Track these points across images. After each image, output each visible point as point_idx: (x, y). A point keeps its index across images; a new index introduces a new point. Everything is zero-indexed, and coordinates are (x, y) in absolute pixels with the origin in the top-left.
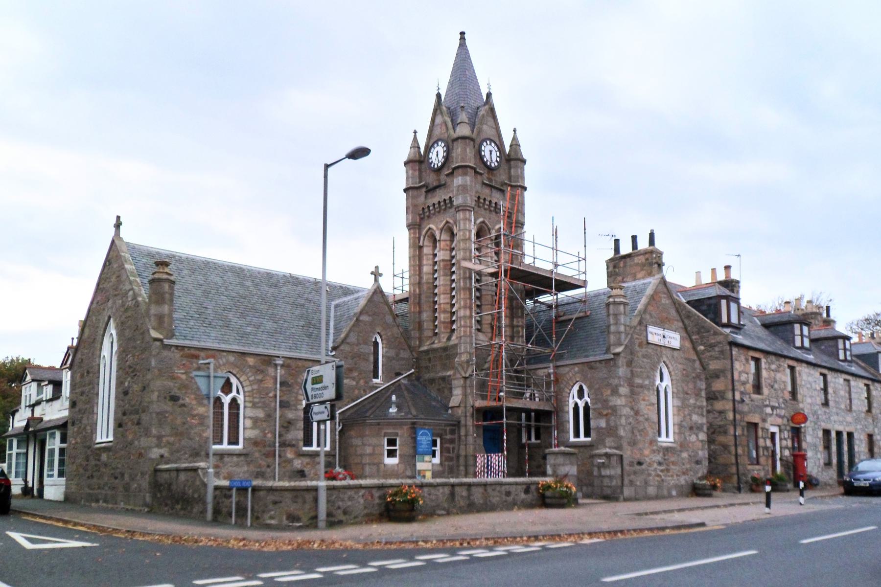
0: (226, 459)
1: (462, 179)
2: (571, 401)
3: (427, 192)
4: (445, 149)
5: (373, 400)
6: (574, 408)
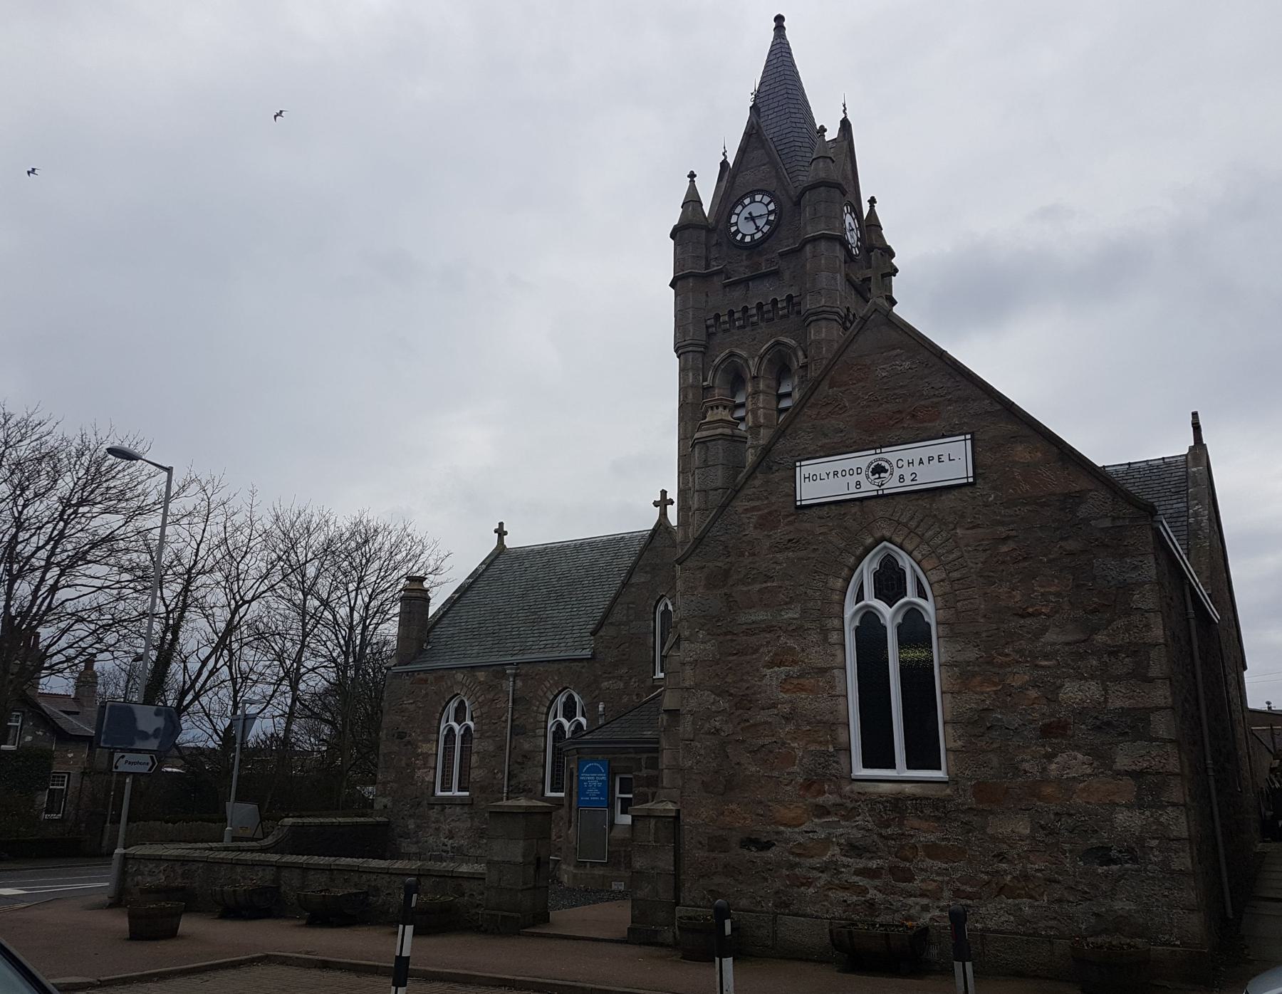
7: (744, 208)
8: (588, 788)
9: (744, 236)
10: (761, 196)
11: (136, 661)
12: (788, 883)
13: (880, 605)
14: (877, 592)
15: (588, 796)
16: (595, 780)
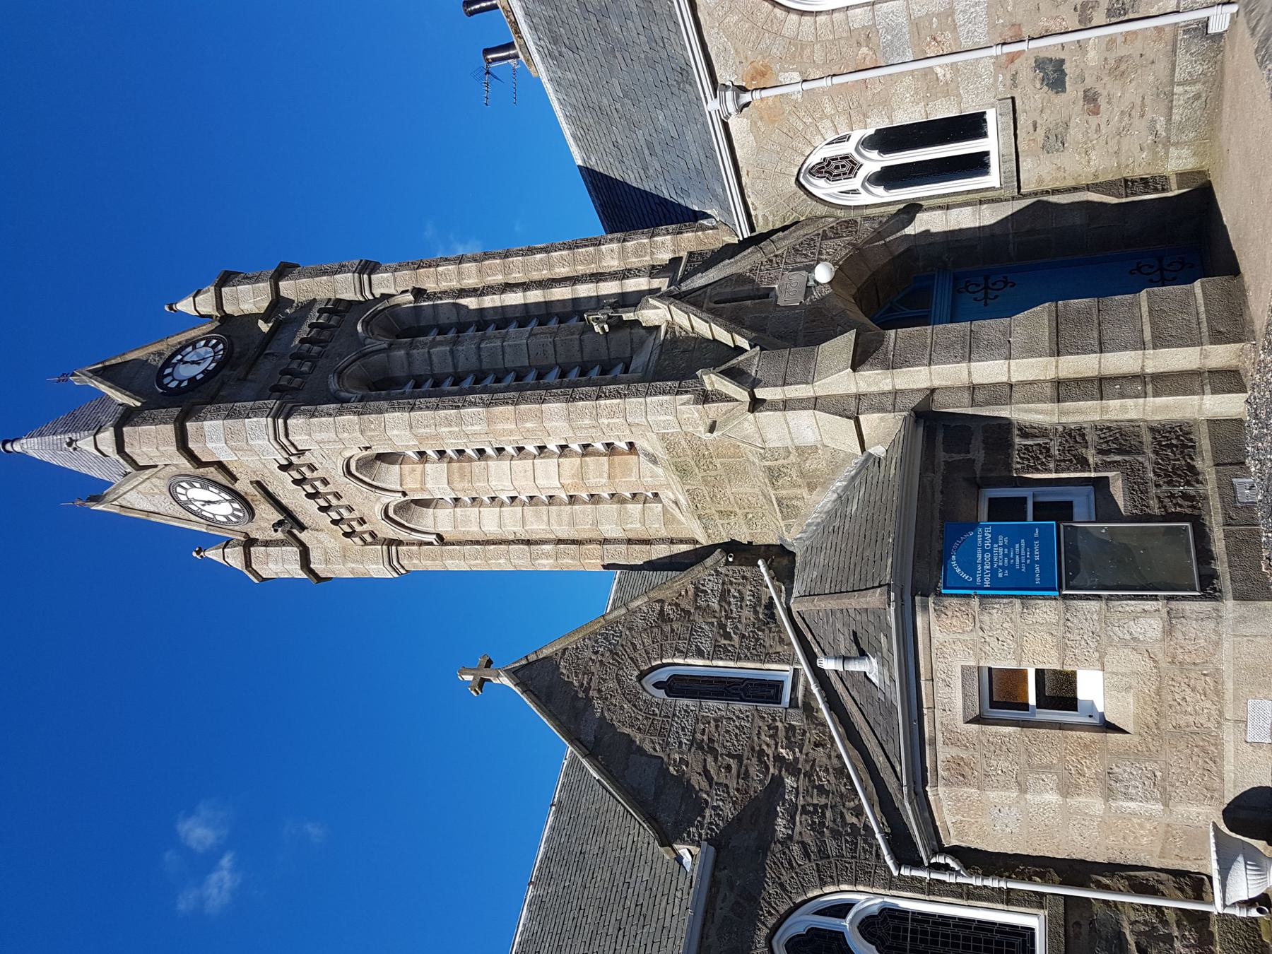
0: (771, 548)
2: (864, 199)
3: (302, 528)
5: (709, 694)
6: (889, 187)
8: (1011, 567)
11: (745, 88)
12: (1118, 386)
13: (862, 174)
15: (1030, 568)
16: (991, 551)
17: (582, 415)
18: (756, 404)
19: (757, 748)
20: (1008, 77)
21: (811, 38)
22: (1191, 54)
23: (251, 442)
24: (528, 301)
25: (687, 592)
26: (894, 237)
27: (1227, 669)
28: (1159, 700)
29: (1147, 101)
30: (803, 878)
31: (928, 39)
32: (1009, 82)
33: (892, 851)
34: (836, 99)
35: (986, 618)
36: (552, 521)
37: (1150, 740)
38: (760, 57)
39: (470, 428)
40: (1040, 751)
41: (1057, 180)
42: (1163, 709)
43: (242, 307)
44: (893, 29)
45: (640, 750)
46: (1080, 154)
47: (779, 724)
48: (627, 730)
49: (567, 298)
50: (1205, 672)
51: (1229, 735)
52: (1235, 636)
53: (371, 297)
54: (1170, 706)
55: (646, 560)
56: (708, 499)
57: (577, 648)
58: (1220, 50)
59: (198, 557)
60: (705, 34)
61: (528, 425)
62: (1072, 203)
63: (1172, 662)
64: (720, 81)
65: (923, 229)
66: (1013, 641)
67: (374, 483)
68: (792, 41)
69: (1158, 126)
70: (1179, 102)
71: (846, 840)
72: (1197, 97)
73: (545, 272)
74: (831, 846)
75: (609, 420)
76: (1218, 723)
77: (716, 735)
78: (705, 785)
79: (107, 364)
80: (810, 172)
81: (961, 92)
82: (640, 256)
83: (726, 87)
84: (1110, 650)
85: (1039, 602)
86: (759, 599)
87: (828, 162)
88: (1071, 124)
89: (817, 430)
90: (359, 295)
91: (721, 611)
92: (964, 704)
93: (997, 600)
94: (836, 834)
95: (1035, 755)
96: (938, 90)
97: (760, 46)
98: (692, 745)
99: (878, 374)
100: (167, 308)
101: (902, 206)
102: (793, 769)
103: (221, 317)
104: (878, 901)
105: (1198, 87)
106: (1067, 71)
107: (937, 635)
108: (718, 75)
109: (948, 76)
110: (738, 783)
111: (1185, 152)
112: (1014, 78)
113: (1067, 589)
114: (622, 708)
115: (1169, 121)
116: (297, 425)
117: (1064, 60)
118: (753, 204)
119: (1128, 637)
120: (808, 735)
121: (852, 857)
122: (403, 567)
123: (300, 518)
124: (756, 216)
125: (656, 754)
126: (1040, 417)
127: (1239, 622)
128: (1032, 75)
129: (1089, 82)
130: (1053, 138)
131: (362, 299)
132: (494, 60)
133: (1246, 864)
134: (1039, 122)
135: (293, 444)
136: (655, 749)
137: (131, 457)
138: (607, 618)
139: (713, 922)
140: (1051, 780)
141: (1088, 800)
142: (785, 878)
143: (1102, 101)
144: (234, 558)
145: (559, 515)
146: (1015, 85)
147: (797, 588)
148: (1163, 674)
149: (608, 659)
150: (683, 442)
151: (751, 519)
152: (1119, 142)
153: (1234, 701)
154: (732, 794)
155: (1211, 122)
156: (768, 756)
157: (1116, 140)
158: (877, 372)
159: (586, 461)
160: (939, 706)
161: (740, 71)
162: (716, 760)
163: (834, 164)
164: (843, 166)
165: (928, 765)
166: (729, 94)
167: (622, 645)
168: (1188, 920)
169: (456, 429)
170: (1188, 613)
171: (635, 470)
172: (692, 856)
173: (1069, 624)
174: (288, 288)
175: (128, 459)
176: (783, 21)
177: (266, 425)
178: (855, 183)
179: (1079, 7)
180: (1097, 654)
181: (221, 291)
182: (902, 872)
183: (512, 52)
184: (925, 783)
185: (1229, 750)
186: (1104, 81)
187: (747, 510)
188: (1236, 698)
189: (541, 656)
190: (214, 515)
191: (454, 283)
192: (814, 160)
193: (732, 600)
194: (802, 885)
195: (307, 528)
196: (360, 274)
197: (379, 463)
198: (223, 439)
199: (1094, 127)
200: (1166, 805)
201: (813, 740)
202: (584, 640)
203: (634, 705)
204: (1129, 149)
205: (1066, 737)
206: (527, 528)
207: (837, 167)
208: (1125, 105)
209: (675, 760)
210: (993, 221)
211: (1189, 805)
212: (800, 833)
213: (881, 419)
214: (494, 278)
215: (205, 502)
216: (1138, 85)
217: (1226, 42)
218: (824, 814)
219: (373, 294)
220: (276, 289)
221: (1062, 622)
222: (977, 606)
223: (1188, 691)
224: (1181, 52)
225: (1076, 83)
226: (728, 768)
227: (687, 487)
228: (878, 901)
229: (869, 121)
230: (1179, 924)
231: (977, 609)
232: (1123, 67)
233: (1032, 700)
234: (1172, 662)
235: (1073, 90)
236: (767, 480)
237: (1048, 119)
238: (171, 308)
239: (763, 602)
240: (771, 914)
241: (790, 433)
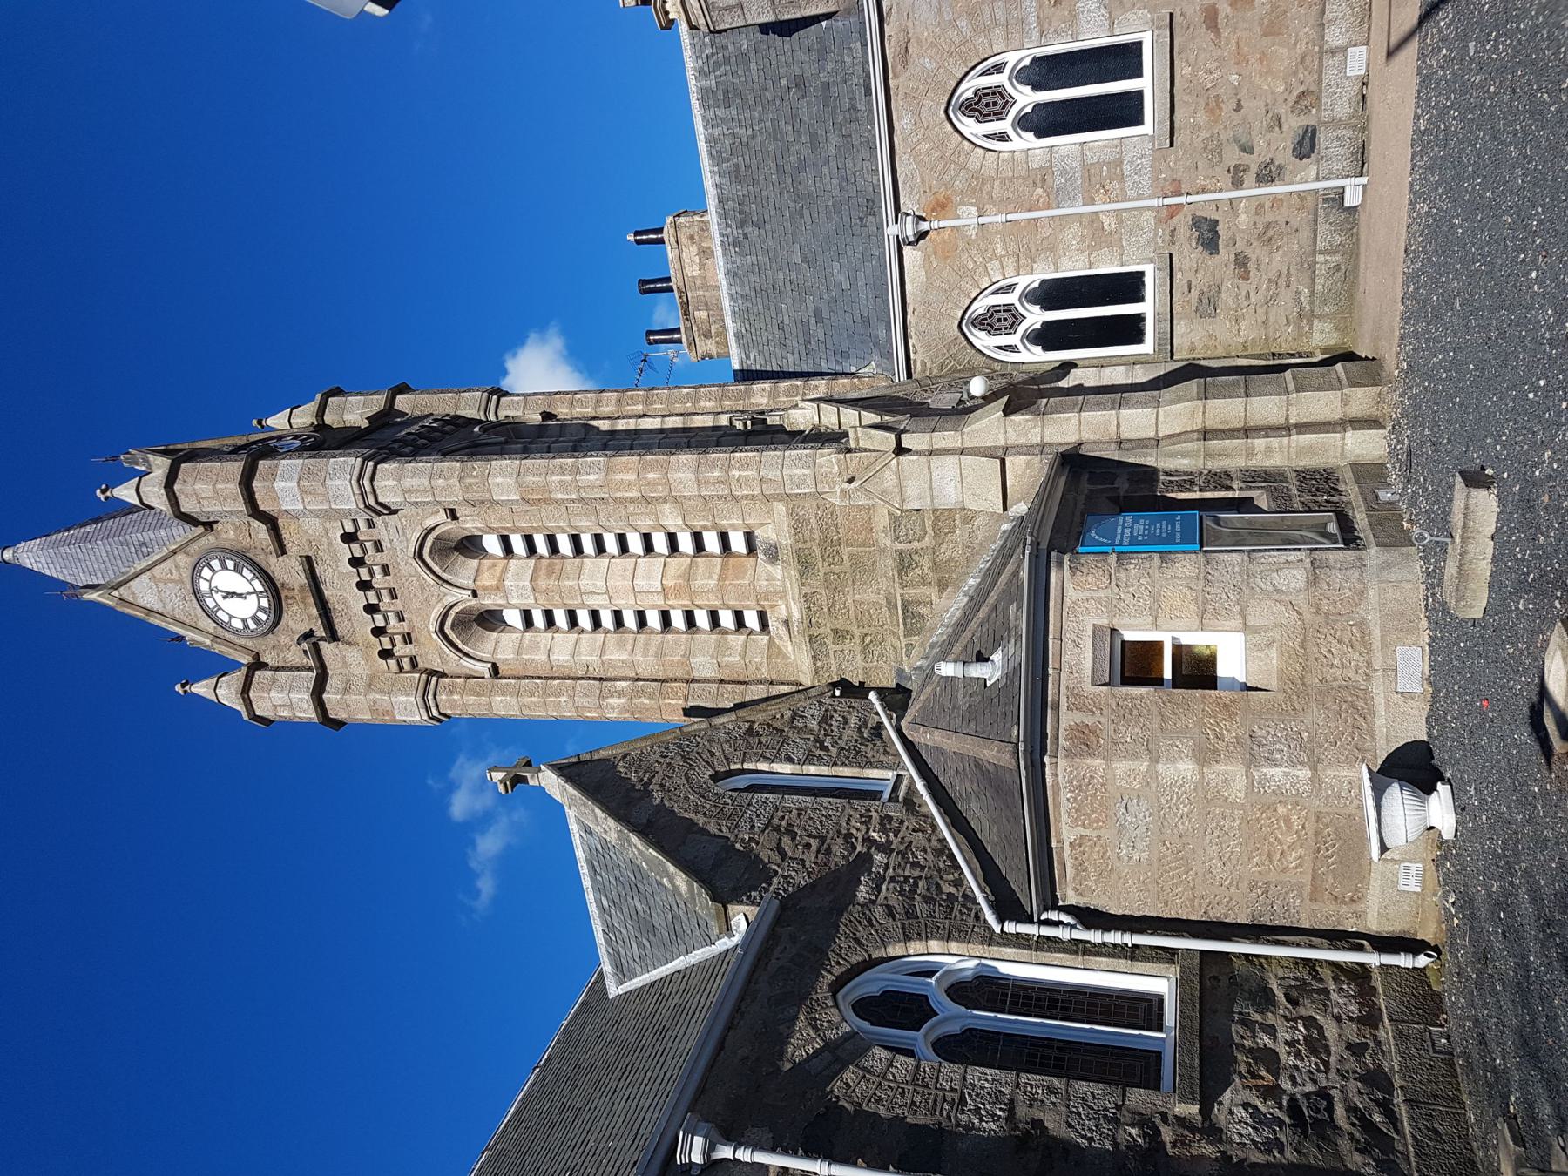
1: (283, 479)
3: (333, 636)
4: (230, 564)
7: (220, 608)
9: (260, 608)
10: (201, 580)
13: (1021, 329)
14: (1157, 1042)
17: (713, 467)
18: (900, 450)
19: (844, 831)
20: (1167, 232)
21: (992, 173)
22: (1330, 224)
23: (328, 482)
24: (665, 426)
25: (782, 716)
26: (1048, 386)
27: (1374, 618)
28: (1302, 651)
29: (1293, 271)
30: (884, 935)
31: (1098, 186)
32: (1167, 238)
33: (994, 907)
34: (1008, 240)
35: (1123, 575)
36: (637, 651)
37: (1295, 698)
38: (943, 187)
39: (585, 477)
40: (1175, 714)
41: (1208, 348)
42: (1308, 663)
43: (345, 417)
44: (1067, 173)
45: (703, 831)
46: (1230, 321)
47: (873, 814)
48: (687, 815)
49: (706, 425)
50: (1351, 623)
51: (1378, 687)
52: (1382, 582)
53: (493, 418)
54: (1316, 659)
55: (737, 702)
56: (826, 610)
57: (642, 753)
58: (1355, 223)
59: (181, 692)
60: (897, 159)
61: (651, 476)
62: (1222, 368)
63: (1317, 613)
64: (903, 209)
65: (1076, 383)
66: (1150, 596)
67: (444, 575)
68: (975, 175)
69: (1302, 298)
70: (1321, 271)
71: (940, 905)
72: (1337, 268)
73: (689, 405)
74: (922, 909)
75: (741, 473)
76: (1367, 675)
77: (798, 821)
78: (778, 859)
79: (171, 447)
80: (972, 323)
81: (1124, 243)
82: (792, 396)
83: (907, 215)
84: (1253, 603)
85: (1179, 555)
86: (866, 724)
87: (993, 310)
88: (1224, 288)
89: (959, 485)
90: (482, 413)
91: (820, 730)
92: (1093, 666)
93: (1135, 555)
94: (927, 899)
95: (1170, 719)
96: (1103, 239)
97: (945, 176)
98: (766, 828)
99: (1027, 420)
100: (255, 422)
101: (1057, 364)
102: (886, 848)
103: (318, 425)
104: (972, 963)
105: (1338, 257)
106: (1220, 233)
107: (1071, 593)
108: (902, 202)
109: (1113, 226)
110: (817, 857)
111: (1328, 326)
112: (1173, 233)
113: (1207, 546)
114: (687, 798)
115: (1312, 292)
116: (387, 470)
117: (1217, 221)
118: (914, 346)
119: (1271, 588)
120: (906, 823)
121: (946, 918)
122: (437, 706)
123: (336, 621)
124: (915, 360)
125: (721, 834)
126: (1185, 461)
127: (1383, 568)
128: (1189, 233)
129: (1240, 246)
130: (1205, 301)
131: (483, 418)
132: (656, 342)
133: (1401, 789)
134: (1193, 283)
135: (374, 492)
136: (720, 830)
137: (176, 498)
138: (684, 729)
139: (765, 970)
140: (1185, 745)
141: (1229, 768)
142: (862, 933)
143: (1252, 266)
144: (226, 692)
145: (647, 645)
146: (1173, 242)
147: (908, 717)
148: (1308, 626)
149: (678, 761)
150: (813, 520)
151: (868, 645)
152: (1267, 313)
153: (1382, 648)
154: (808, 866)
155: (1351, 297)
156: (856, 839)
157: (1263, 310)
158: (1027, 417)
159: (696, 562)
160: (1065, 668)
161: (923, 200)
162: (793, 839)
163: (996, 316)
164: (1005, 320)
165: (1048, 731)
166: (909, 219)
167: (698, 753)
168: (1345, 976)
169: (569, 478)
170: (1331, 563)
171: (750, 572)
172: (748, 924)
173: (1210, 577)
174: (403, 403)
175: (172, 497)
176: (968, 155)
177: (353, 466)
178: (1014, 339)
179: (1232, 169)
180: (1238, 608)
181: (327, 400)
182: (1006, 929)
183: (676, 336)
184: (1043, 751)
185: (1380, 702)
186: (1253, 246)
187: (865, 631)
188: (1384, 645)
189: (596, 757)
190: (231, 617)
191: (589, 410)
192: (980, 307)
193: (834, 723)
194: (882, 940)
195: (339, 640)
196: (489, 394)
197: (456, 554)
198: (296, 477)
199: (1244, 293)
200: (1314, 769)
201: (911, 827)
202: (652, 747)
203: (704, 797)
204: (1276, 321)
205: (1205, 697)
206: (604, 658)
207: (999, 320)
208: (1272, 275)
209: (743, 840)
210: (1144, 380)
211: (1339, 768)
212: (886, 898)
213: (1028, 463)
214: (634, 407)
215: (228, 593)
216: (1284, 255)
217: (1362, 216)
218: (916, 884)
219: (497, 417)
220: (391, 402)
221: (1202, 575)
222: (1114, 562)
223: (1335, 643)
224: (1321, 220)
225: (1228, 246)
226: (808, 846)
227: (806, 590)
228: (972, 963)
229: (1035, 266)
230: (1335, 979)
231: (1114, 565)
232: (1270, 233)
233: (1167, 674)
234: (1317, 613)
235: (1225, 254)
236: (896, 572)
237: (1201, 281)
238: (260, 422)
239: (870, 725)
240: (838, 963)
241: (931, 488)
